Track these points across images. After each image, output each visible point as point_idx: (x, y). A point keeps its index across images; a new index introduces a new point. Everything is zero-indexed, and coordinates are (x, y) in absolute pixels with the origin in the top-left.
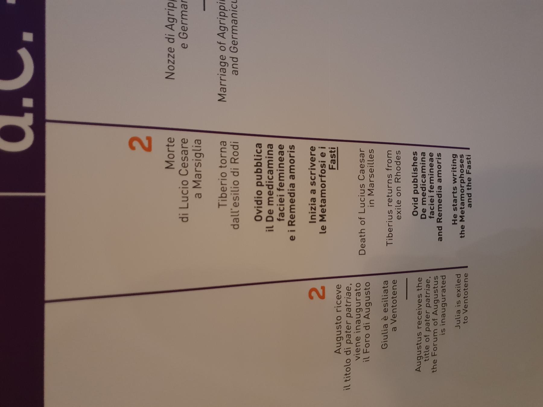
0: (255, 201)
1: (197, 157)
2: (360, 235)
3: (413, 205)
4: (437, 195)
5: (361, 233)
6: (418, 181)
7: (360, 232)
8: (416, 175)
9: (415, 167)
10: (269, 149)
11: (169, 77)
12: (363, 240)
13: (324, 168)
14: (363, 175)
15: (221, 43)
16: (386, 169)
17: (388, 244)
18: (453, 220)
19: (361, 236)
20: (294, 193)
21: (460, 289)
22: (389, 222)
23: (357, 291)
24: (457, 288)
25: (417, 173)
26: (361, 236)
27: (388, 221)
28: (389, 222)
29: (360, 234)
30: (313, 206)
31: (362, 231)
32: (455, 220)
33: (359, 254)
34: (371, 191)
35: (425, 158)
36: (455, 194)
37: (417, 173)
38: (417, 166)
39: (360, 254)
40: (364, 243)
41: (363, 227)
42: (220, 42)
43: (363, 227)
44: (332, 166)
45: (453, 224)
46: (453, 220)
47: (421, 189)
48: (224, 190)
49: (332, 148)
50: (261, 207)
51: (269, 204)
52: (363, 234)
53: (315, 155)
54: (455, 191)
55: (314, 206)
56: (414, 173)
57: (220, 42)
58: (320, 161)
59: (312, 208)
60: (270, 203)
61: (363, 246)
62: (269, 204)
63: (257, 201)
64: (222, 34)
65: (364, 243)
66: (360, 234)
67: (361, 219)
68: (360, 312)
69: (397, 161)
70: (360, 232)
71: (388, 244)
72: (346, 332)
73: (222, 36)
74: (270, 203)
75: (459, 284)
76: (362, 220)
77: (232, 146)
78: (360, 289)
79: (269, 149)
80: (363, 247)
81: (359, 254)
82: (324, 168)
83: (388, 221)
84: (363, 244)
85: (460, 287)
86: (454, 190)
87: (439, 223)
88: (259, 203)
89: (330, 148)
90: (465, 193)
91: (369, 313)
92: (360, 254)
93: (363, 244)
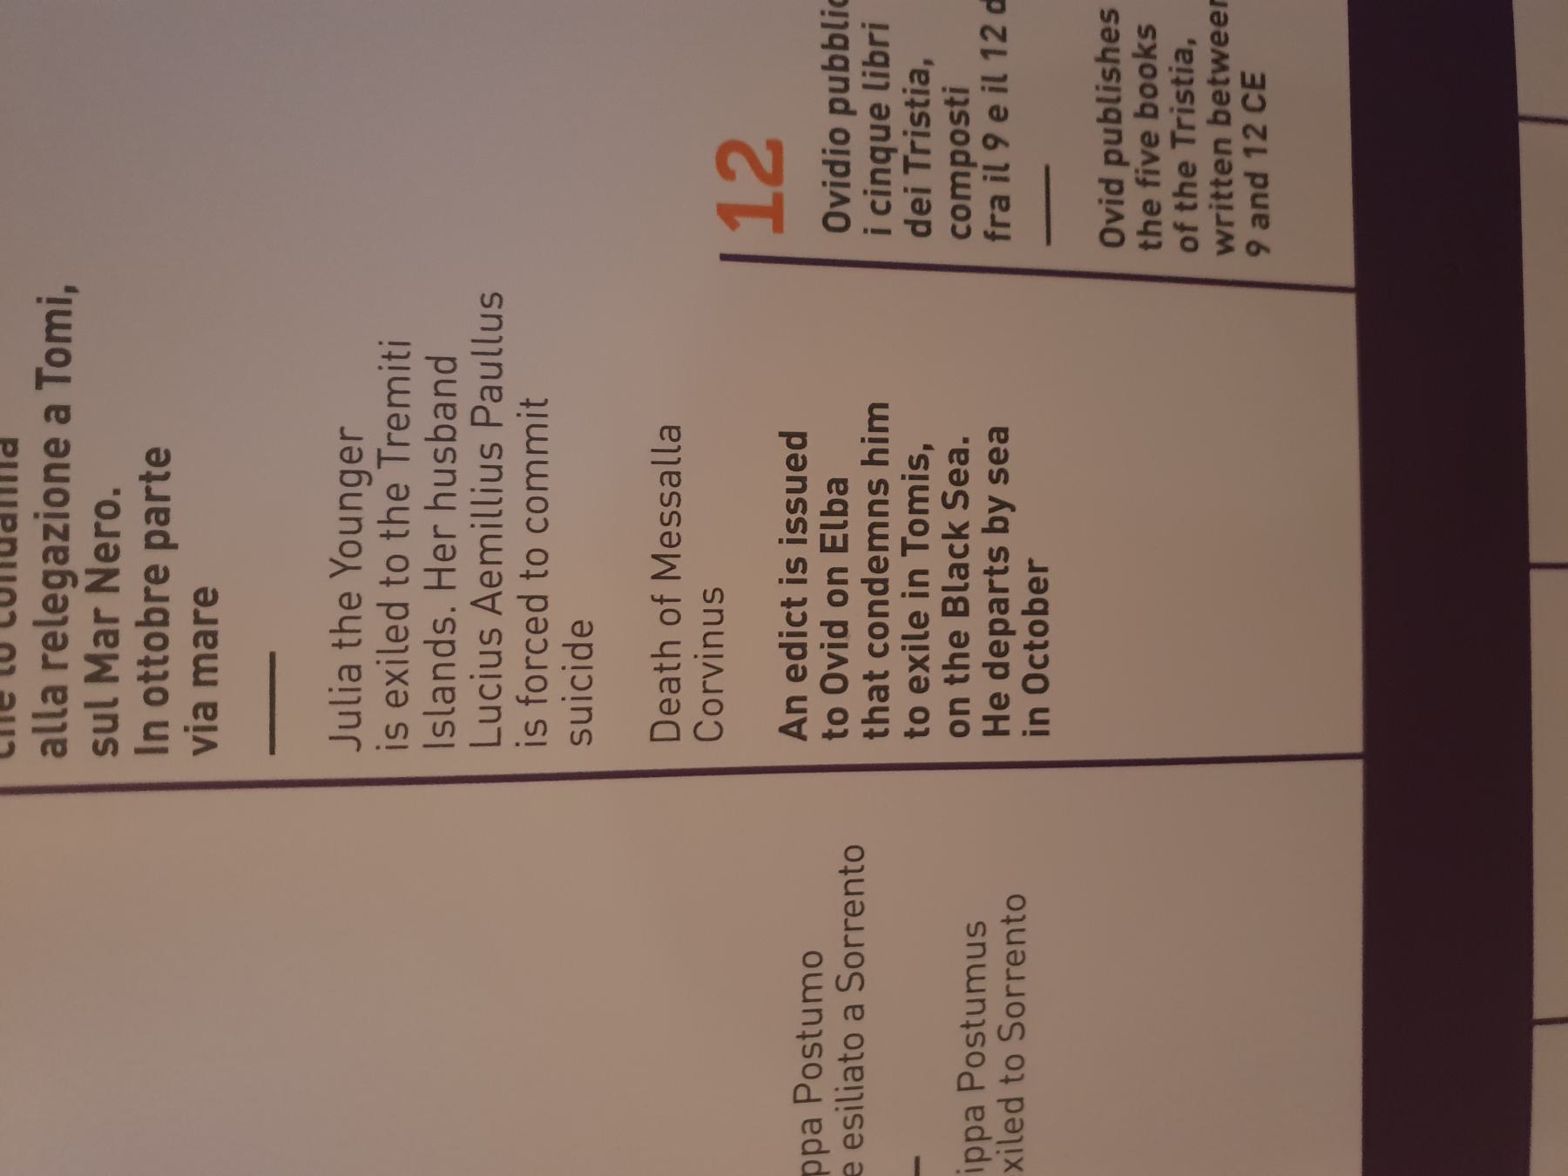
3: (826, 650)
6: (849, 510)
7: (432, 505)
8: (841, 522)
14: (716, 723)
15: (665, 597)
17: (536, 628)
18: (986, 718)
19: (661, 669)
20: (847, 165)
21: (1020, 1160)
22: (574, 668)
26: (661, 669)
29: (657, 662)
30: (58, 524)
31: (667, 649)
32: (996, 719)
33: (652, 739)
34: (666, 562)
35: (886, 709)
36: (995, 578)
39: (655, 736)
40: (674, 697)
42: (662, 596)
45: (986, 733)
46: (986, 718)
47: (866, 586)
48: (398, 494)
49: (952, 90)
51: (197, 683)
52: (668, 662)
54: (999, 565)
57: (662, 596)
58: (948, 87)
59: (48, 531)
60: (203, 677)
62: (197, 683)
63: (832, 164)
64: (490, 601)
65: (674, 697)
66: (657, 662)
67: (661, 600)
69: (490, 594)
71: (536, 628)
73: (490, 607)
74: (203, 677)
75: (1016, 1137)
76: (667, 605)
80: (669, 713)
81: (652, 739)
84: (669, 700)
85: (1020, 1150)
86: (995, 560)
92: (655, 736)
93: (669, 700)
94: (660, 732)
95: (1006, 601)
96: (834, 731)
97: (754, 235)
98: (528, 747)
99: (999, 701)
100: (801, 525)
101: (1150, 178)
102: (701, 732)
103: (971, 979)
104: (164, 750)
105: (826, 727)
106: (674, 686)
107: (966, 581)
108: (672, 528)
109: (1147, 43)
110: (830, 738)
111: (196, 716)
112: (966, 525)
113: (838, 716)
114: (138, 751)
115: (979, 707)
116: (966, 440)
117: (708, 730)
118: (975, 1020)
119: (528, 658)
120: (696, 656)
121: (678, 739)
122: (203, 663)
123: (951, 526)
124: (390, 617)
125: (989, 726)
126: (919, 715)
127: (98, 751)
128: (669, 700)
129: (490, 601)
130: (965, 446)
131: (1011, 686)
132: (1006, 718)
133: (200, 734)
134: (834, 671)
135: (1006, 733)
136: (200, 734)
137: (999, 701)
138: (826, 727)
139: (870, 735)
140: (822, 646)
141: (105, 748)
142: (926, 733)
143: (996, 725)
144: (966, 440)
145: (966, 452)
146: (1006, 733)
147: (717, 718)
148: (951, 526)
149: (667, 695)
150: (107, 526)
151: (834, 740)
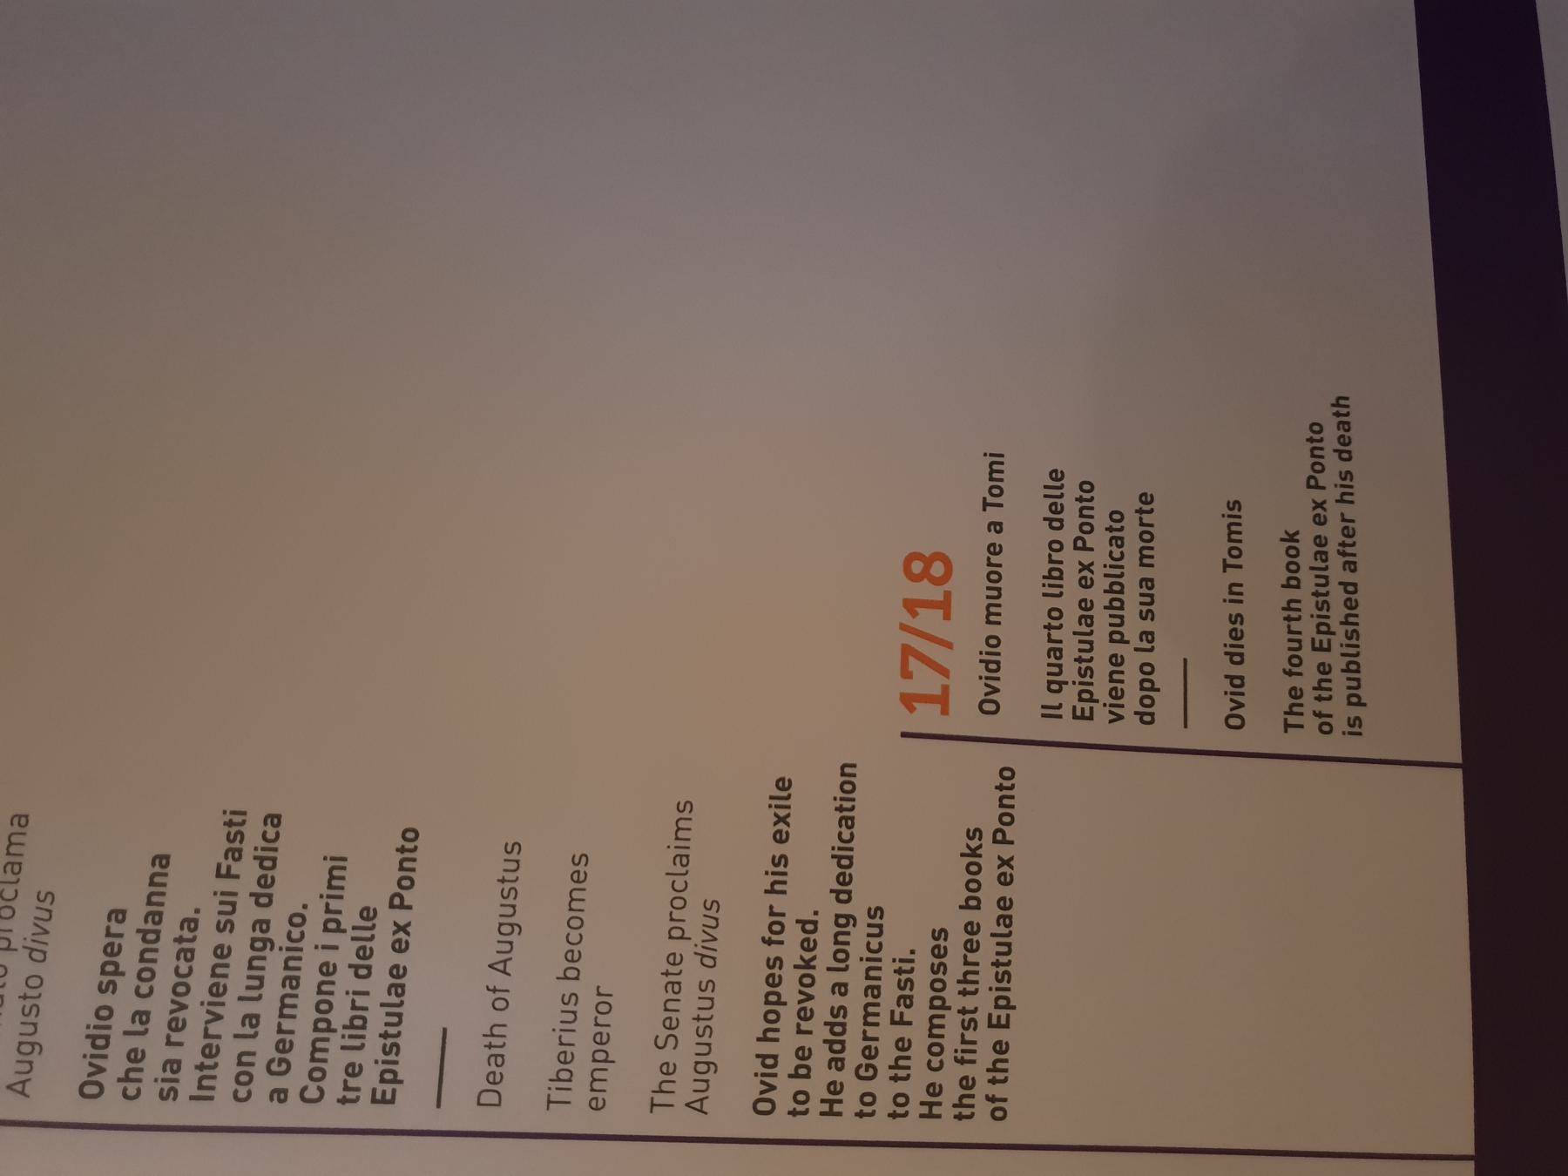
0: (88, 1037)
1: (679, 928)
2: (488, 1044)
4: (257, 862)
5: (493, 1035)
9: (1350, 628)
10: (870, 999)
11: (692, 1105)
12: (498, 1059)
13: (940, 976)
16: (487, 987)
19: (490, 1046)
22: (561, 1030)
23: (497, 993)
24: (773, 810)
25: (1358, 646)
26: (490, 1046)
27: (557, 1030)
28: (561, 1030)
31: (496, 1031)
32: (831, 1102)
33: (479, 1104)
37: (1358, 646)
38: (1357, 624)
40: (498, 1070)
41: (499, 1017)
43: (499, 1017)
44: (902, 1014)
48: (671, 1024)
50: (105, 1057)
52: (495, 1041)
53: (876, 1039)
55: (911, 687)
56: (1348, 646)
61: (494, 1080)
63: (93, 1038)
64: (699, 1103)
67: (495, 990)
68: (511, 936)
69: (608, 1064)
70: (489, 1033)
72: (667, 974)
76: (498, 995)
77: (686, 936)
78: (517, 878)
79: (870, 999)
82: (940, 976)
83: (557, 1030)
87: (831, 1117)
88: (993, 666)
89: (759, 1075)
90: (697, 936)
91: (24, 1077)
92: (482, 1101)
93: (494, 1073)
94: (485, 1098)
95: (878, 988)
96: (348, 1097)
97: (927, 718)
98: (194, 1102)
99: (834, 1088)
100: (978, 834)
101: (967, 1056)
102: (307, 1095)
103: (679, 829)
104: (211, 1098)
105: (892, 1108)
106: (499, 1060)
107: (402, 998)
108: (581, 868)
109: (974, 844)
110: (960, 1119)
111: (164, 1070)
112: (1297, 533)
113: (901, 1100)
114: (192, 1098)
115: (951, 1093)
116: (197, 911)
117: (312, 1093)
118: (704, 1014)
119: (596, 1018)
120: (554, 1030)
121: (499, 1105)
122: (288, 1001)
123: (1286, 532)
124: (681, 928)
125: (925, 1110)
126: (868, 1099)
127: (163, 1096)
128: (494, 1073)
129: (699, 1103)
130: (196, 916)
131: (846, 1076)
132: (840, 1101)
133: (989, 682)
134: (1235, 712)
135: (839, 1114)
136: (989, 682)
137: (834, 1088)
138: (892, 1108)
139: (959, 1117)
140: (202, 1003)
141: (170, 1094)
142: (872, 1114)
143: (831, 1107)
144: (197, 911)
145: (196, 921)
146: (839, 1114)
147: (321, 1084)
148: (1286, 532)
149: (494, 1068)
150: (601, 1020)
151: (347, 1105)
